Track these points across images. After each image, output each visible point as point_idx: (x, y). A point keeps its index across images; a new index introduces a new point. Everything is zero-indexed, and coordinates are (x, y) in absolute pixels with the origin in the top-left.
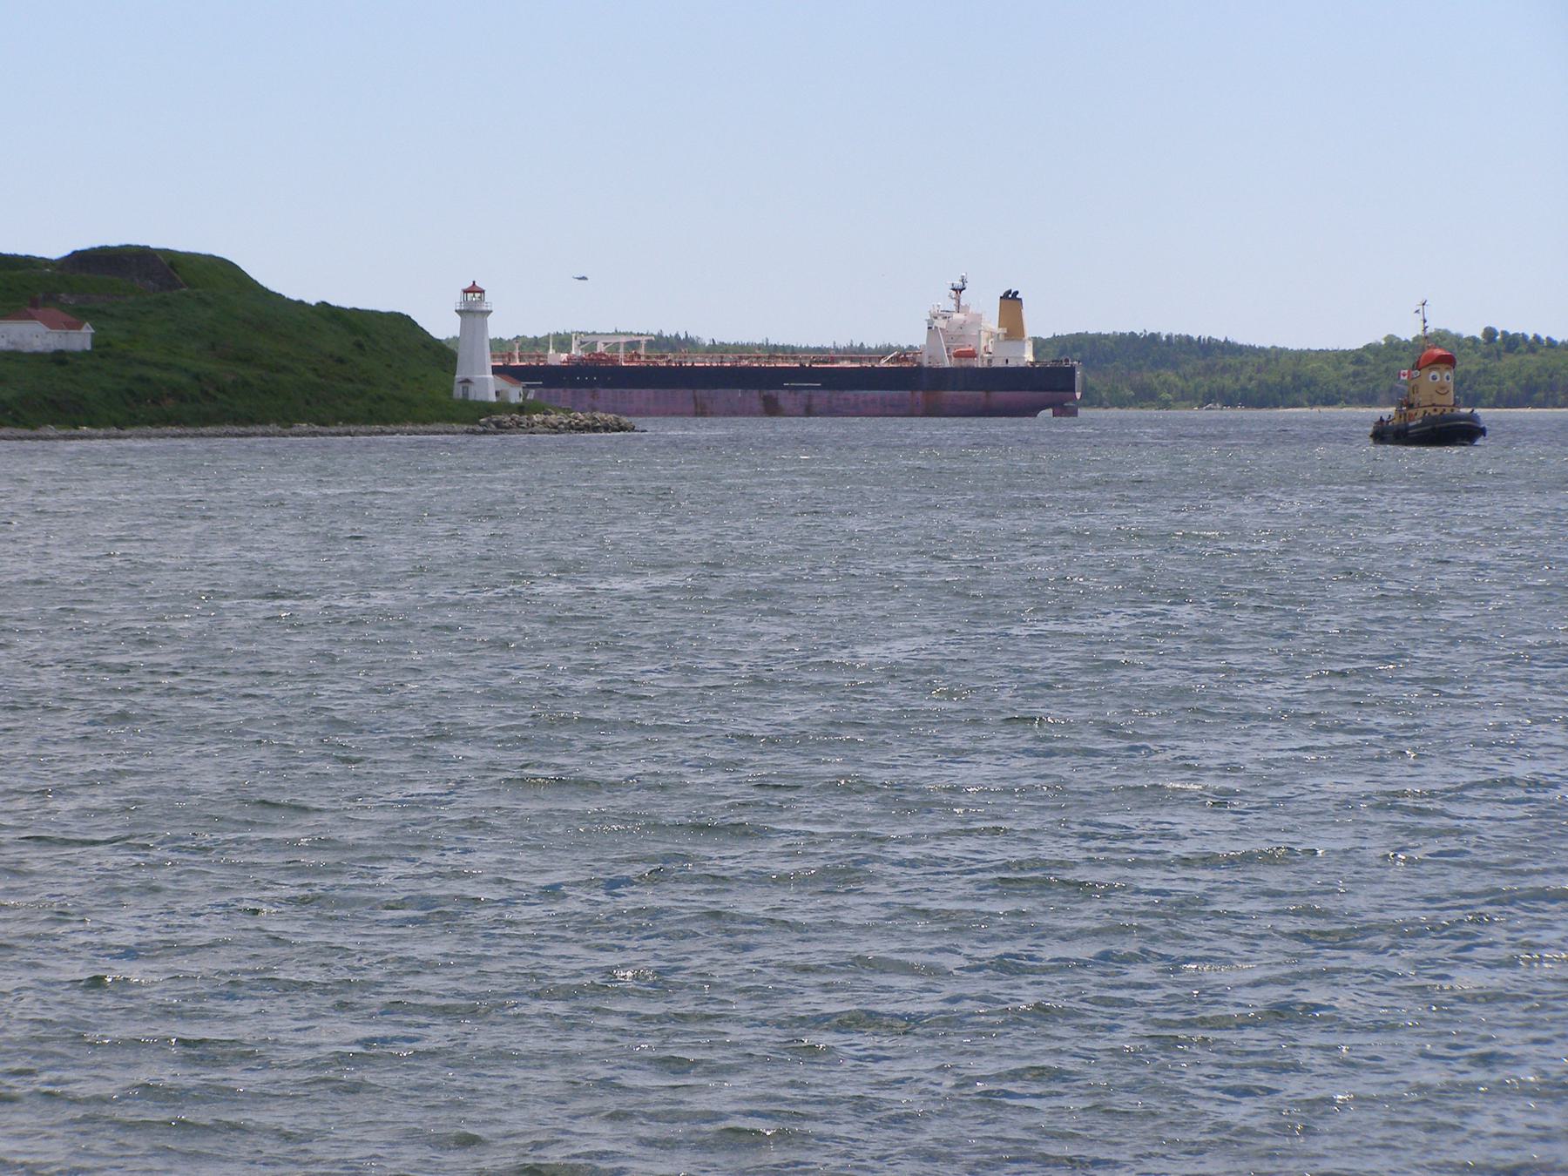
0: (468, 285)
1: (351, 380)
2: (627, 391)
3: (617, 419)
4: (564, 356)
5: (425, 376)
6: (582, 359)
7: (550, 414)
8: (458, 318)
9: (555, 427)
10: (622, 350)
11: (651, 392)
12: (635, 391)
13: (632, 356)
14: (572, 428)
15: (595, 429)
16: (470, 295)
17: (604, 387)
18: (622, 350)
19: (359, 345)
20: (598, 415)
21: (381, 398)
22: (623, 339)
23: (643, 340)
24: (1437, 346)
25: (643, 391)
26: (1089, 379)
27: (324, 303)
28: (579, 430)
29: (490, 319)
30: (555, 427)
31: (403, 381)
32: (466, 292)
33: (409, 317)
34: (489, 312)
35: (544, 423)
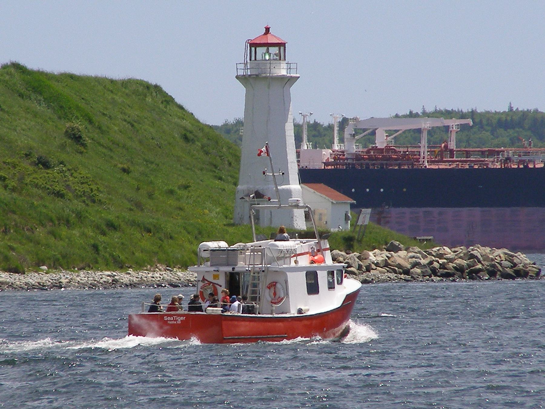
0: (256, 34)
1: (60, 195)
2: (435, 210)
3: (510, 258)
4: (326, 154)
5: (186, 187)
6: (358, 157)
7: (396, 249)
8: (241, 90)
9: (407, 272)
10: (424, 142)
11: (477, 211)
12: (450, 211)
13: (441, 153)
14: (434, 272)
15: (474, 274)
16: (261, 50)
17: (396, 205)
18: (424, 142)
19: (77, 138)
20: (479, 251)
21: (112, 226)
22: (426, 124)
23: (454, 123)
24: (40, 352)
25: (465, 211)
26: (322, 256)
27: (16, 66)
28: (447, 275)
29: (294, 90)
30: (407, 272)
31: (150, 196)
32: (254, 45)
33: (157, 88)
34: (291, 80)
35: (386, 264)
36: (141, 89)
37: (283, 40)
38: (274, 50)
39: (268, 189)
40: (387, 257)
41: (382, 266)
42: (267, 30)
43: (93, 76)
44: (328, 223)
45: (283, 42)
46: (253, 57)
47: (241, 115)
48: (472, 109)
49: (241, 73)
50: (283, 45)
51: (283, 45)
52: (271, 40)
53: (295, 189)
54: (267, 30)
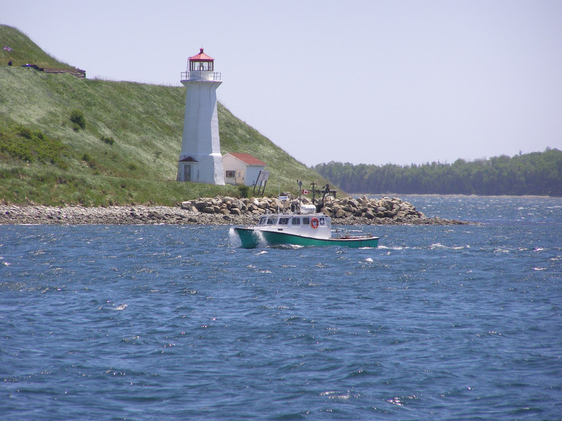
0: (194, 53)
16: (197, 64)
32: (192, 61)
36: (115, 92)
37: (211, 57)
38: (205, 64)
39: (199, 155)
40: (269, 202)
41: (263, 208)
42: (202, 51)
43: (367, 164)
44: (245, 179)
45: (211, 59)
46: (191, 68)
47: (87, 77)
48: (412, 164)
49: (184, 78)
50: (212, 61)
51: (212, 61)
52: (202, 57)
53: (216, 156)
54: (202, 51)
